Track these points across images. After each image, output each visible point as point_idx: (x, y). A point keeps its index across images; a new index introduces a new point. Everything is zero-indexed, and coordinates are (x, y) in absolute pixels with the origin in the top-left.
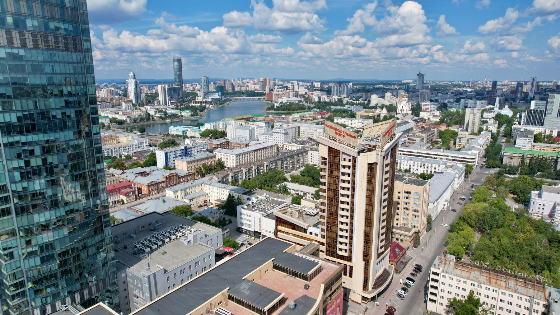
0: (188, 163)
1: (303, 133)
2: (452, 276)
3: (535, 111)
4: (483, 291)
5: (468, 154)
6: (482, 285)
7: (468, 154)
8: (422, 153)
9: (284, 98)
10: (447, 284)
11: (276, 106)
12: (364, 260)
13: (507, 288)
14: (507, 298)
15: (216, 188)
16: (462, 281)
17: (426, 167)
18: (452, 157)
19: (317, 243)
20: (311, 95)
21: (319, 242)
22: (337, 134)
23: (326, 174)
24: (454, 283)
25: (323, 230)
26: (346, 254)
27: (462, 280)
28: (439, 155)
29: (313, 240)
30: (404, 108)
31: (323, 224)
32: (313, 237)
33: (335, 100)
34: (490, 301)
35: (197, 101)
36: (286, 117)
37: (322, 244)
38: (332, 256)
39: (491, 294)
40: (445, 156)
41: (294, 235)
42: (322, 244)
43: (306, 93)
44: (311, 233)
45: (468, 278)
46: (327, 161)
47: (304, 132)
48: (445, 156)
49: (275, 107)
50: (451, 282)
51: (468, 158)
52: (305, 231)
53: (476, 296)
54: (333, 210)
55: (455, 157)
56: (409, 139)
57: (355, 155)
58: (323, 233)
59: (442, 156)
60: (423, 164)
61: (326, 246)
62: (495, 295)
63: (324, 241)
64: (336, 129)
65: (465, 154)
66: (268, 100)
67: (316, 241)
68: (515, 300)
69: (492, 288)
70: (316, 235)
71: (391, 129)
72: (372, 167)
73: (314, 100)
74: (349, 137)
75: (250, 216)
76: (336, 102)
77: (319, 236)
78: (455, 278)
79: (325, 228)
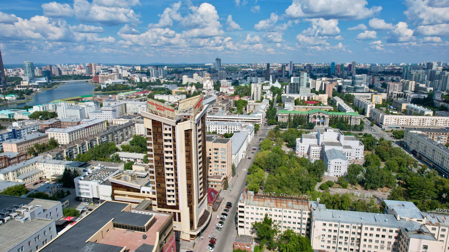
0: (18, 144)
1: (129, 109)
2: (252, 207)
3: (294, 84)
4: (273, 213)
5: (255, 117)
6: (272, 209)
7: (255, 117)
8: (224, 119)
9: (110, 80)
10: (250, 213)
11: (103, 87)
12: (188, 206)
13: (287, 207)
14: (288, 214)
15: (51, 165)
16: (259, 209)
17: (227, 129)
18: (245, 119)
19: (149, 199)
20: (133, 77)
21: (151, 198)
22: (158, 109)
23: (152, 142)
24: (255, 211)
25: (153, 188)
26: (174, 204)
27: (259, 208)
28: (236, 119)
29: (146, 197)
30: (208, 85)
31: (153, 183)
32: (146, 195)
33: (154, 80)
34: (278, 219)
35: (22, 85)
36: (113, 96)
37: (154, 199)
38: (163, 207)
39: (278, 213)
40: (240, 119)
41: (129, 196)
42: (154, 199)
43: (129, 76)
44: (144, 192)
45: (263, 206)
46: (152, 131)
47: (130, 108)
48: (240, 119)
49: (102, 88)
50: (253, 211)
51: (255, 120)
52: (138, 191)
53: (269, 218)
54: (160, 171)
55: (247, 119)
56: (213, 109)
57: (174, 125)
58: (154, 191)
59: (238, 119)
60: (225, 127)
61: (158, 201)
62: (280, 214)
63: (155, 196)
64: (157, 105)
65: (253, 117)
66: (95, 83)
67: (149, 198)
68: (292, 215)
69: (278, 209)
70: (148, 193)
71: (200, 102)
72: (188, 133)
73: (136, 80)
74: (168, 111)
75: (87, 185)
76: (155, 82)
77: (151, 193)
78: (255, 207)
79: (155, 186)
